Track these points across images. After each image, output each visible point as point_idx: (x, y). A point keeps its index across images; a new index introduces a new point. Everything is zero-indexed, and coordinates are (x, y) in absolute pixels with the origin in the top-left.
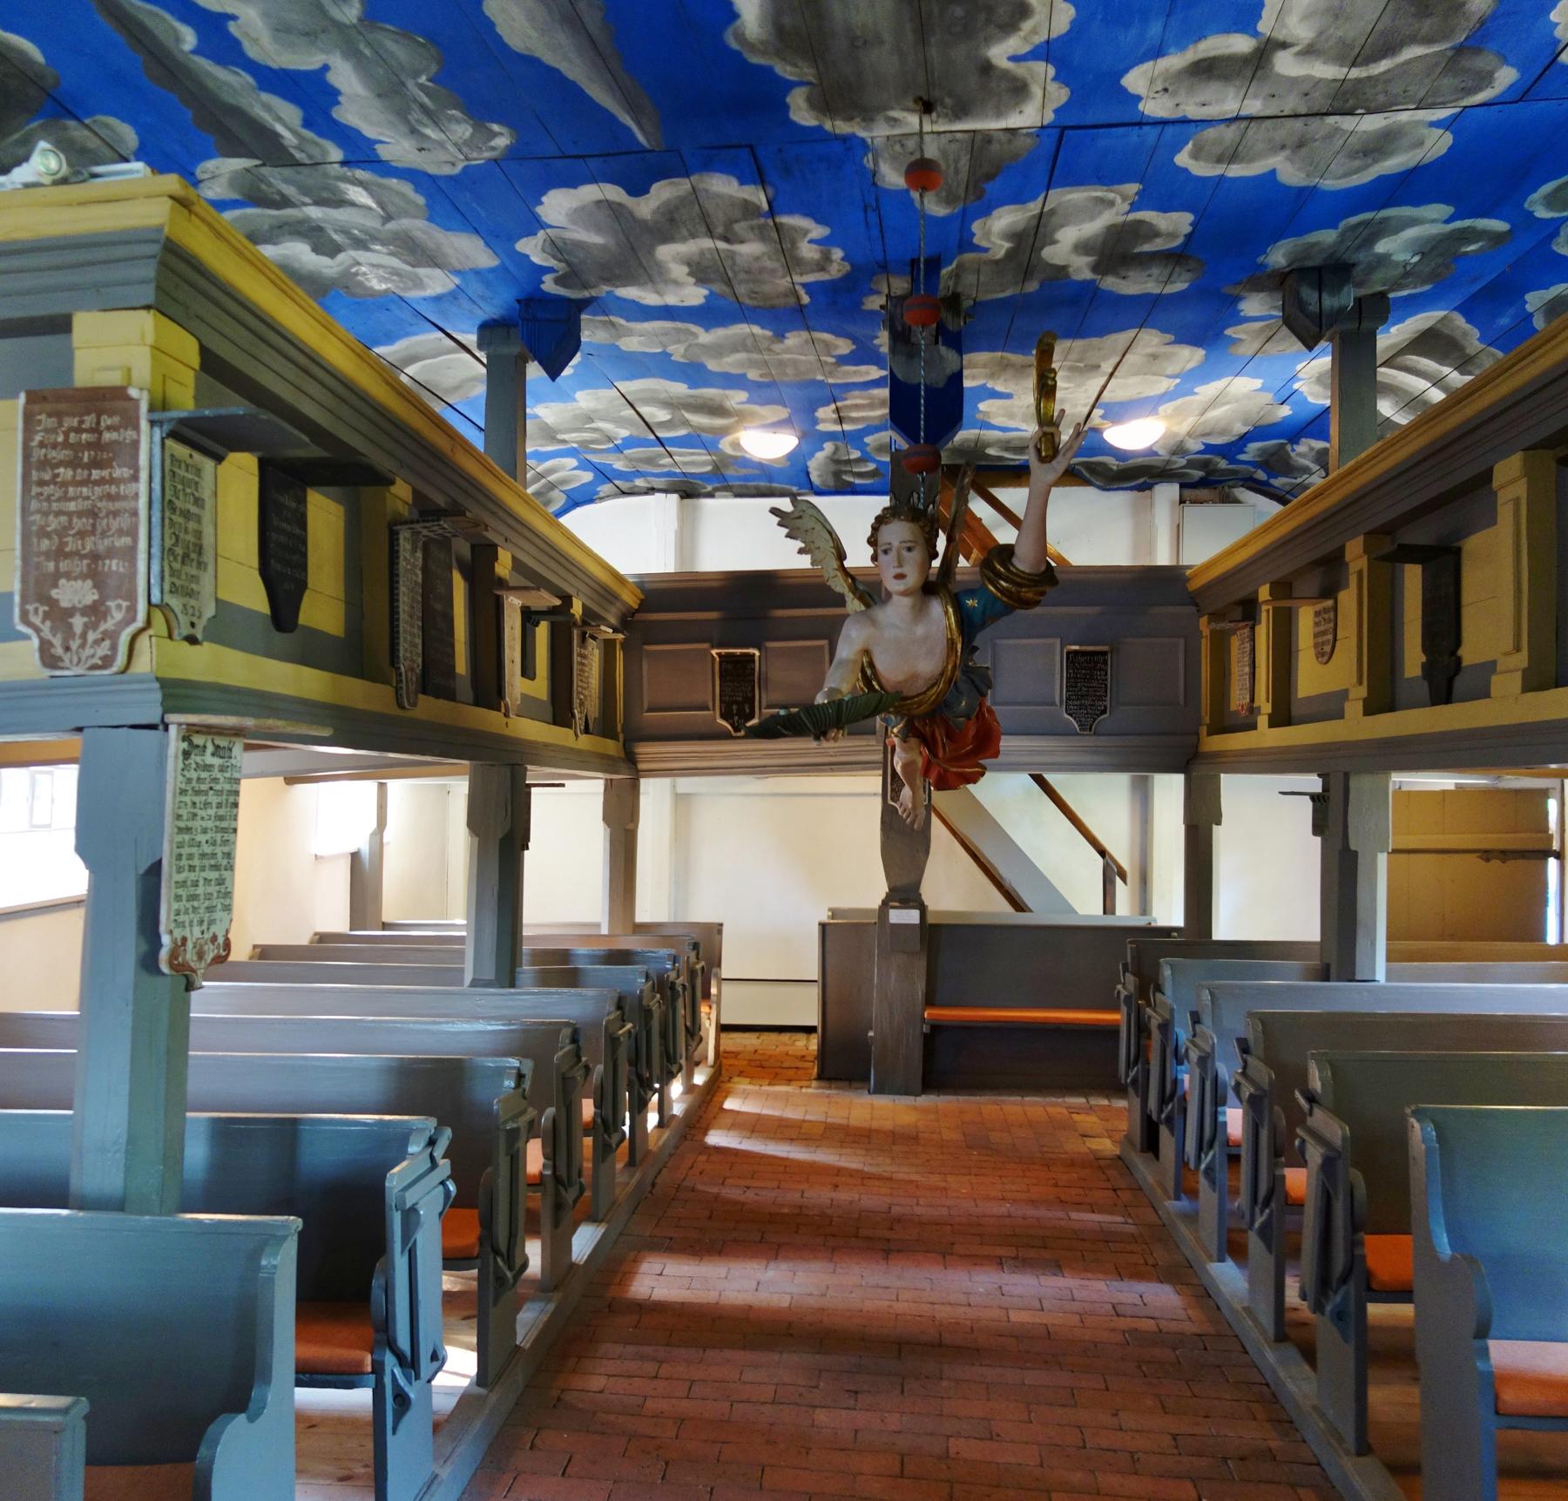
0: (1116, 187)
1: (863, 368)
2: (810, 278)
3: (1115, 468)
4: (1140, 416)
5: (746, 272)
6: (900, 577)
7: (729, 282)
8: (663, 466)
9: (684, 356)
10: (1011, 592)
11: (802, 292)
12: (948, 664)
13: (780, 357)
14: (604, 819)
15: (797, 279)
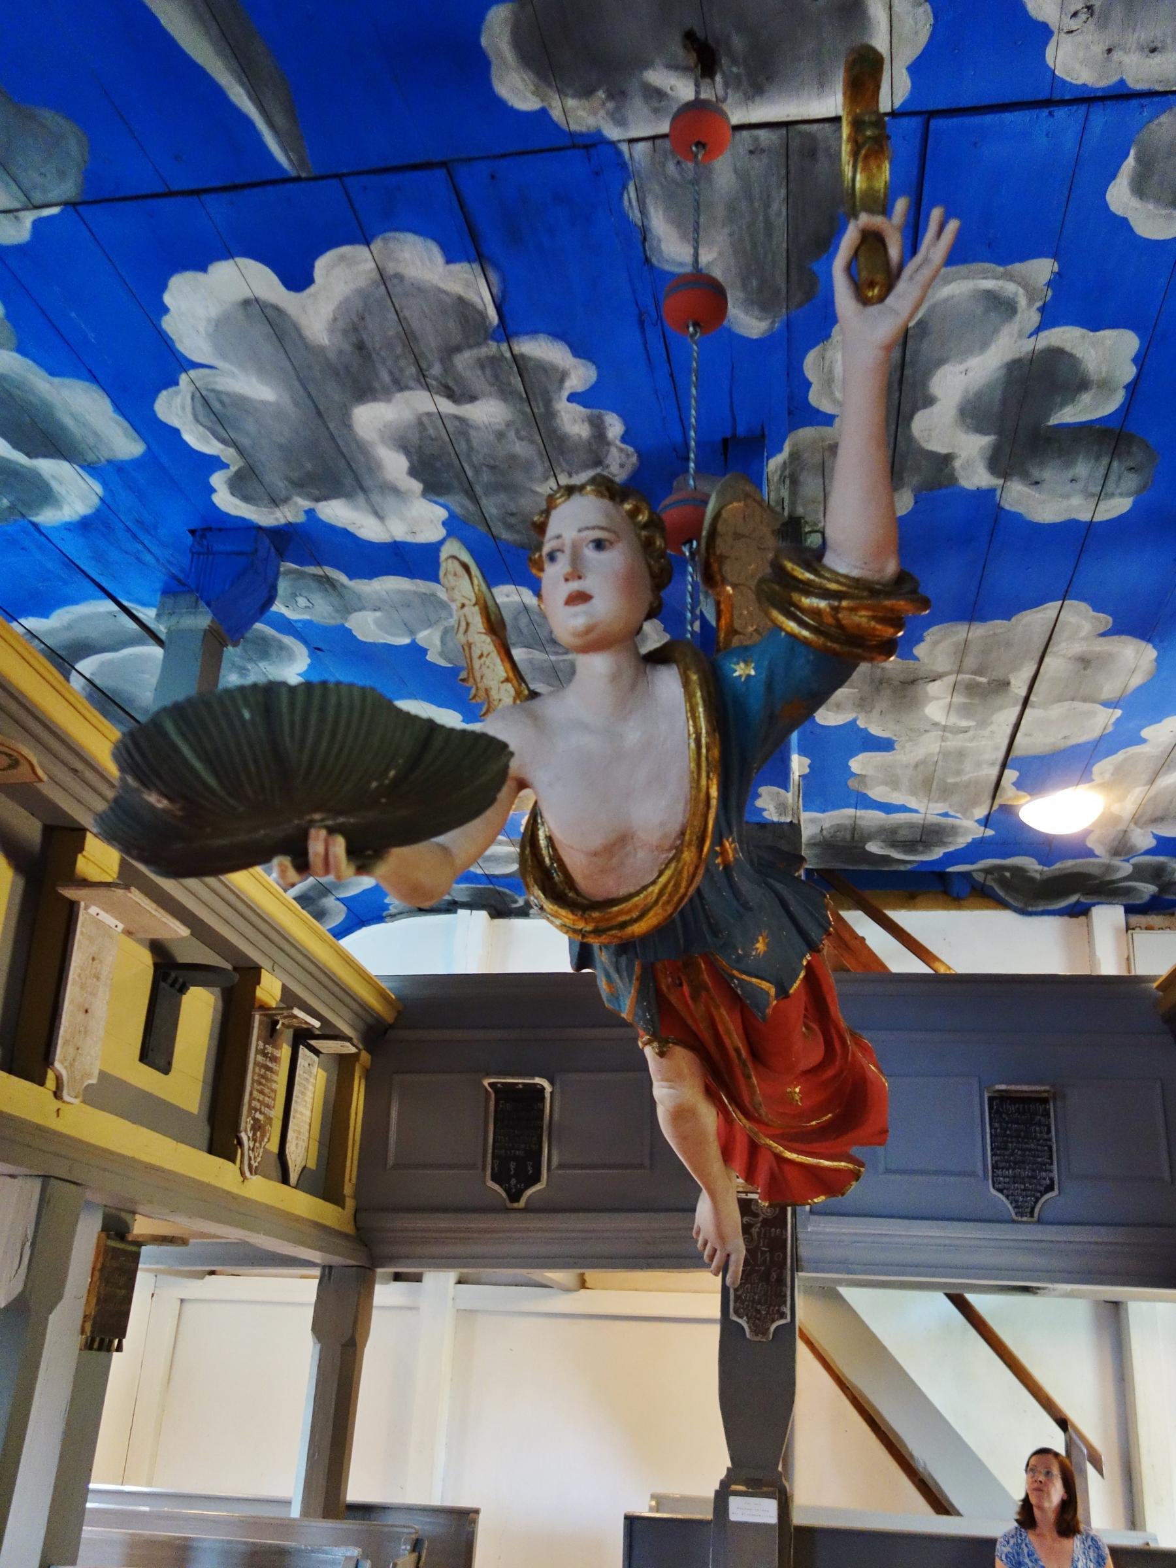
0: (1018, 267)
3: (1038, 876)
4: (1065, 784)
6: (579, 598)
14: (313, 1329)
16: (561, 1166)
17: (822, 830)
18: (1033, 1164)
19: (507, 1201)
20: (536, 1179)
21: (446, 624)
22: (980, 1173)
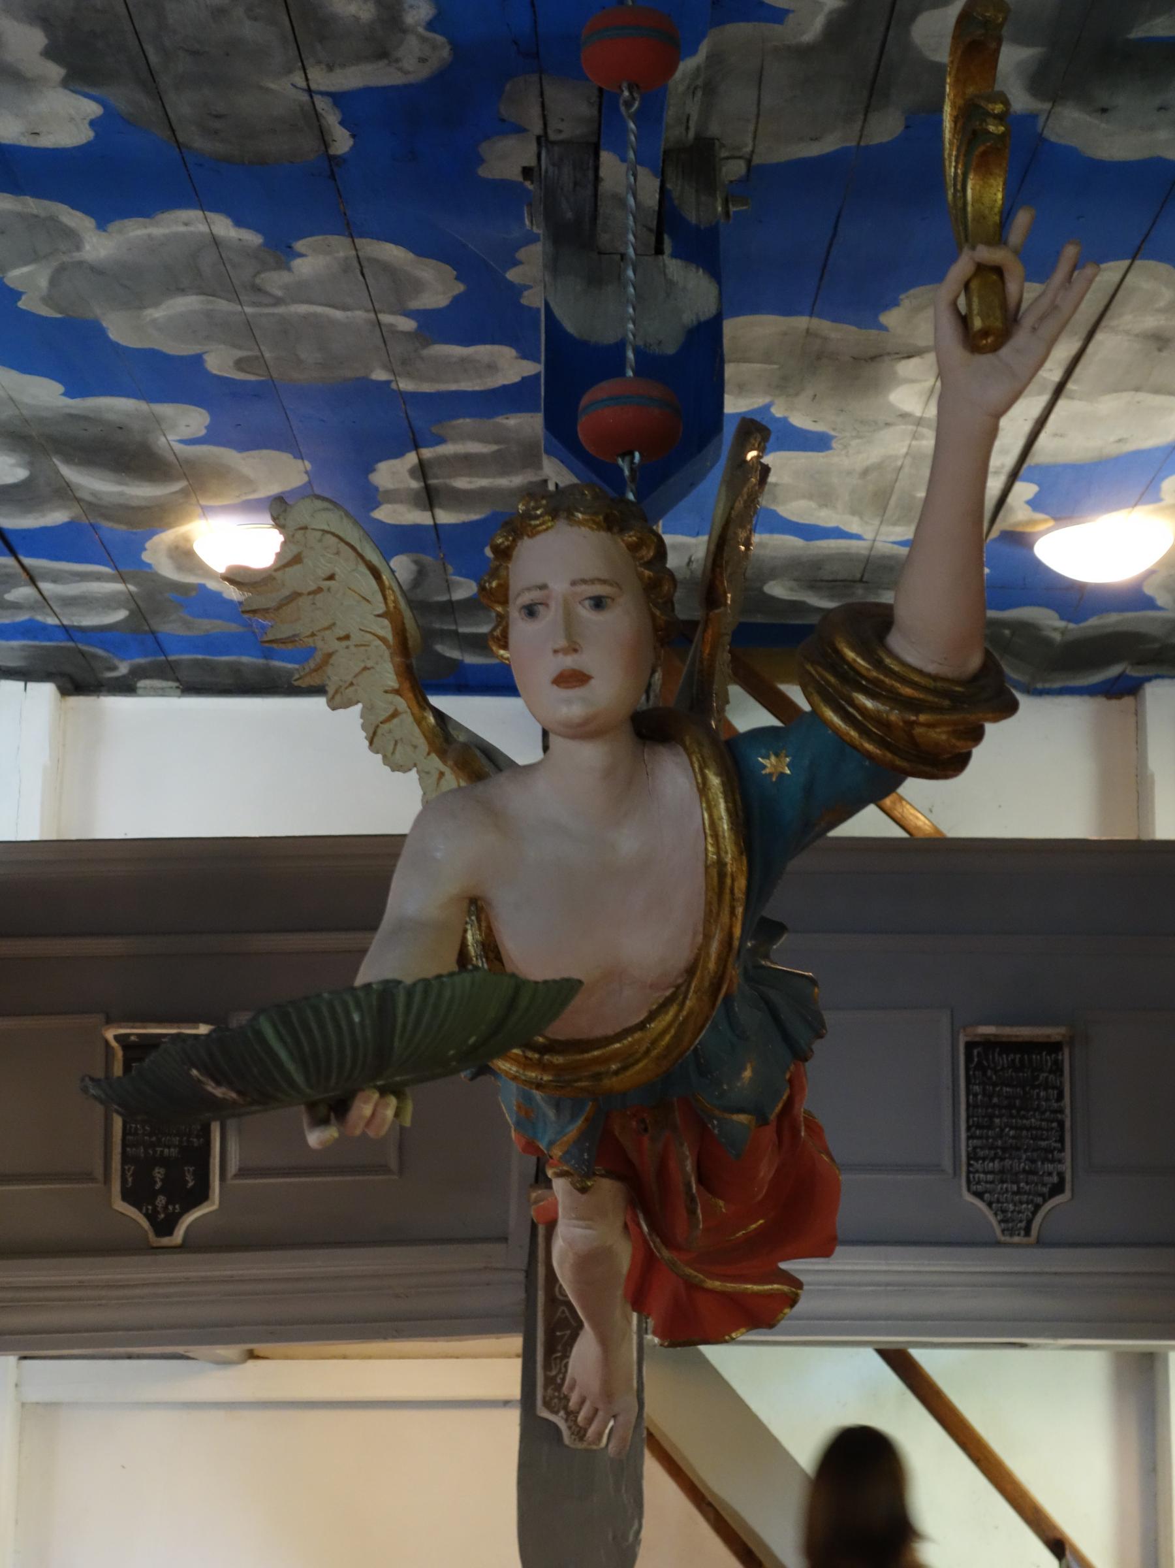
1: (482, 351)
2: (351, 78)
3: (1057, 637)
5: (195, 53)
7: (150, 82)
8: (16, 606)
9: (48, 300)
10: (886, 725)
11: (332, 119)
12: (707, 937)
13: (280, 310)
15: (321, 79)
16: (243, 1172)
17: (690, 562)
18: (1034, 1150)
19: (151, 1235)
20: (201, 1195)
21: (66, 258)
22: (947, 1163)
